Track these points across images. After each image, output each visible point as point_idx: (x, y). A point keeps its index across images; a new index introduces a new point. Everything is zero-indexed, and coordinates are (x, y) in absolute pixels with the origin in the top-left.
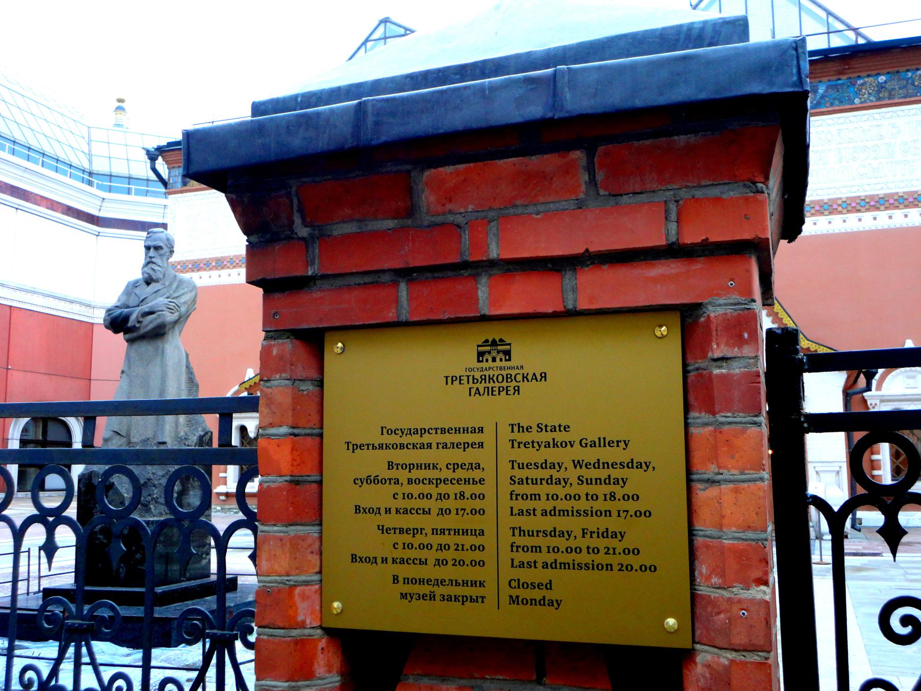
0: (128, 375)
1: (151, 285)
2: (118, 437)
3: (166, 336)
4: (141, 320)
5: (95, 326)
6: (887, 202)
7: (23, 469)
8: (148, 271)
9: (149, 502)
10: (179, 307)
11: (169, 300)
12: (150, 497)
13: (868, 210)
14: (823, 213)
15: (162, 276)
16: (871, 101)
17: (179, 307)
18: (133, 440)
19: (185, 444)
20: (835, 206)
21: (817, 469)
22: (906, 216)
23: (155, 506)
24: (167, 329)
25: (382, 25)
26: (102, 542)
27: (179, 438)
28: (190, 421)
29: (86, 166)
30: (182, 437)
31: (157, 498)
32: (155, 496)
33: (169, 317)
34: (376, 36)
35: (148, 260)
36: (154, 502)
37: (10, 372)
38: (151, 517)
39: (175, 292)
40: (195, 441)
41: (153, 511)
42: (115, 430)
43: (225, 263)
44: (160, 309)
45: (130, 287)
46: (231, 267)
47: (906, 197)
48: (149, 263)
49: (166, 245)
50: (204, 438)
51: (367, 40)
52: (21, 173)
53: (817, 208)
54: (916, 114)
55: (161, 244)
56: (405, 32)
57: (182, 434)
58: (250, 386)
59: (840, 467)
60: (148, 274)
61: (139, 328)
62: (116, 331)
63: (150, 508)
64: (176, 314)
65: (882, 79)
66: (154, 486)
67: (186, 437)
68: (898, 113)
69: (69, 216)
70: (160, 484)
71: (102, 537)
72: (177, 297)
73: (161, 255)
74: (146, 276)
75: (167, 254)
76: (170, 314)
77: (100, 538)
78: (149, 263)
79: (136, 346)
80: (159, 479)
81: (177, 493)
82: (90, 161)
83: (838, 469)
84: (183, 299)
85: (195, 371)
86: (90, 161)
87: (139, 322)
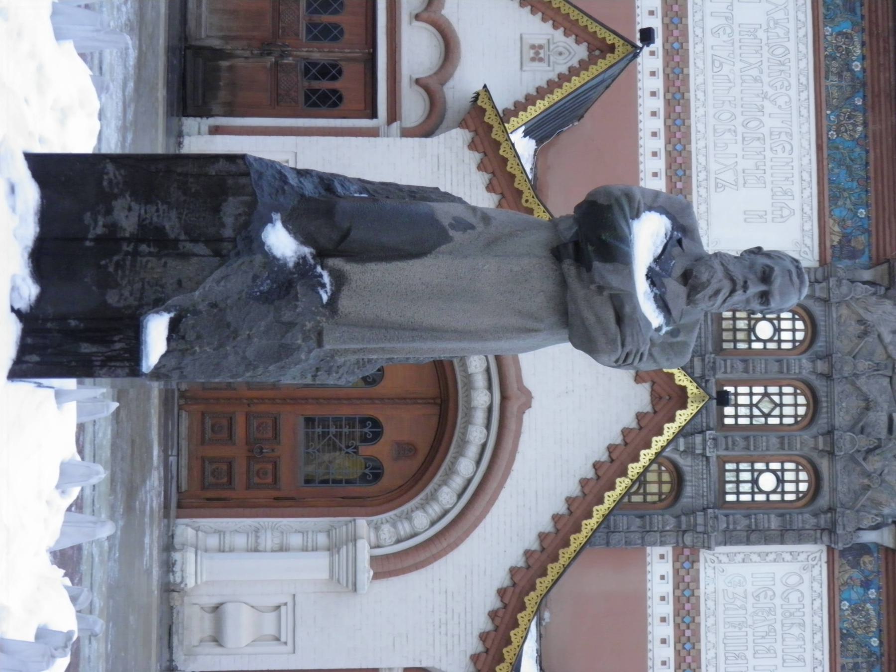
6: (675, 52)
8: (714, 281)
13: (678, 653)
14: (669, 117)
16: (826, 49)
20: (677, 58)
21: (283, 609)
22: (662, 577)
44: (629, 339)
47: (693, 600)
48: (733, 281)
53: (688, 633)
54: (799, 52)
59: (286, 643)
60: (709, 281)
65: (861, 213)
67: (334, 369)
68: (809, 190)
83: (283, 639)
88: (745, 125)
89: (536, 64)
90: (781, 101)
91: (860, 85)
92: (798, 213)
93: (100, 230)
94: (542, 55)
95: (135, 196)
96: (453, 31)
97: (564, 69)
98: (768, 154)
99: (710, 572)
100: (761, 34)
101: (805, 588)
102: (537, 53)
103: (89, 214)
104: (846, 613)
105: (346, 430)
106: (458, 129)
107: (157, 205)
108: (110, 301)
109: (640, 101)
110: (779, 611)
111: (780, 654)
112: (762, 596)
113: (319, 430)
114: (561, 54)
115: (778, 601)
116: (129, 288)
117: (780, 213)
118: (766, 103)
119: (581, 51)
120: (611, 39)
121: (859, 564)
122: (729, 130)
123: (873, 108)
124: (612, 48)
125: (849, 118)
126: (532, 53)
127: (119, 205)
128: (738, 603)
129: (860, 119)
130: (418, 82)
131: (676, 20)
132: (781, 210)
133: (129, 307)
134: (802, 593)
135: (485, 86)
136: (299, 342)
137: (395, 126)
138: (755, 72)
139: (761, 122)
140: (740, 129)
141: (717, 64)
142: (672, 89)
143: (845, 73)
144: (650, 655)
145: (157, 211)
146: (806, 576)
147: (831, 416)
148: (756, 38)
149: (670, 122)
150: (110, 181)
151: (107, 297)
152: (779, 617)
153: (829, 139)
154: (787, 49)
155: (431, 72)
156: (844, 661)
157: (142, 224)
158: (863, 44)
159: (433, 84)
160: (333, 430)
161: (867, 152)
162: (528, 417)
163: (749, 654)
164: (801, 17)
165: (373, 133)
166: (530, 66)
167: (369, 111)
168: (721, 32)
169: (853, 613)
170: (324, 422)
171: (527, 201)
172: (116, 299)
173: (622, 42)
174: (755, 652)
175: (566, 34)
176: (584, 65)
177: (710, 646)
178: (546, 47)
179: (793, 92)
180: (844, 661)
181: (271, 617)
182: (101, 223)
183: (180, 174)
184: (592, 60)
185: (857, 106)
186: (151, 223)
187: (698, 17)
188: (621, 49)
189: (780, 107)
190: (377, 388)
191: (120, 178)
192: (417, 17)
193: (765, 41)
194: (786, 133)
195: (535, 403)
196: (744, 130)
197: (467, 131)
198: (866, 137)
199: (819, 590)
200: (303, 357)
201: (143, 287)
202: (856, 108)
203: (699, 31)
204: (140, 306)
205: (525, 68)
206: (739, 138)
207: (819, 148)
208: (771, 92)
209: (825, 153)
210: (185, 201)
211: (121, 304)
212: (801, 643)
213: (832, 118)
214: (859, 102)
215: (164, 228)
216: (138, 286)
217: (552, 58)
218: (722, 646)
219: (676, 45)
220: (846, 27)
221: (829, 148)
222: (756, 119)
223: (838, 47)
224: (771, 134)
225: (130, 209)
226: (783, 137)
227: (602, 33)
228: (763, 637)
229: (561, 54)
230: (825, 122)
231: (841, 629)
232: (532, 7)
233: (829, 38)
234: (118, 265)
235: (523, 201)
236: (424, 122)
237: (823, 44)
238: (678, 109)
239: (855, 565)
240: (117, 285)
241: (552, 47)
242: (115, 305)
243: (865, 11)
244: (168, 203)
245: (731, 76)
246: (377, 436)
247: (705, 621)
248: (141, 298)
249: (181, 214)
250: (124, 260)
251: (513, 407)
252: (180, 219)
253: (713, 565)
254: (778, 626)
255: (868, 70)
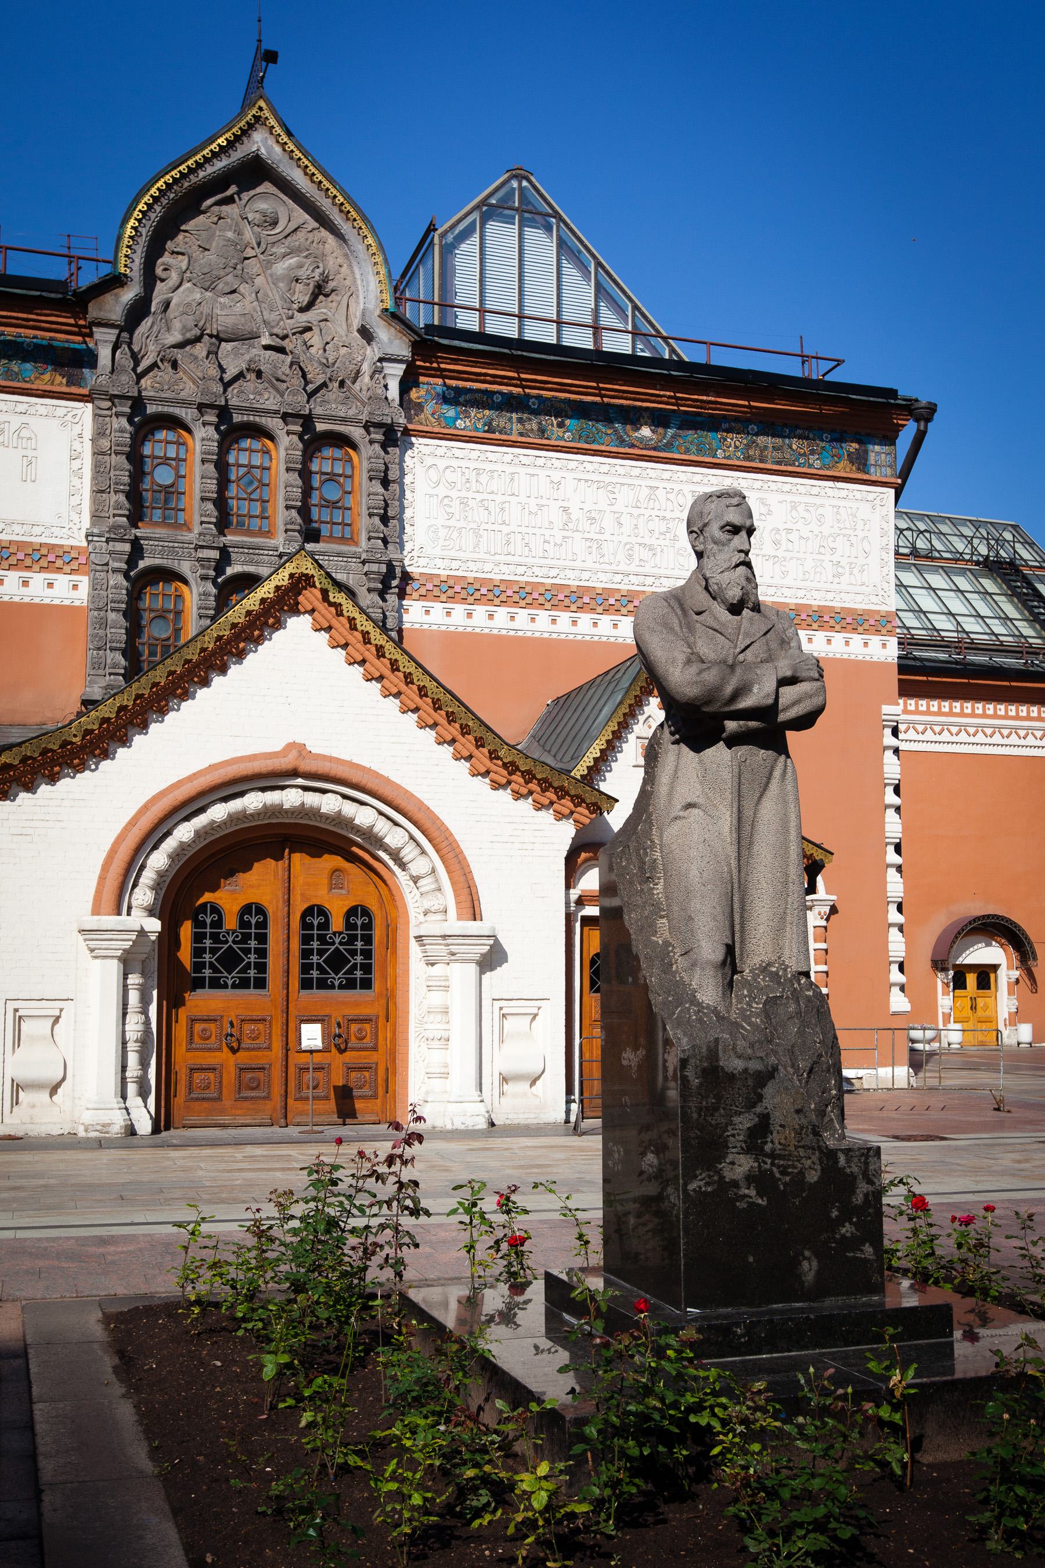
22: (50, 585)
83: (535, 1011)
92: (24, 419)
93: (752, 1192)
95: (721, 1158)
99: (422, 562)
101: (442, 463)
103: (738, 1204)
104: (468, 424)
105: (208, 943)
107: (728, 1136)
108: (815, 1179)
110: (464, 494)
111: (507, 498)
112: (449, 510)
113: (315, 974)
115: (454, 494)
116: (803, 1161)
117: (25, 440)
121: (420, 403)
127: (729, 1175)
128: (455, 535)
132: (22, 438)
133: (820, 1159)
134: (447, 468)
142: (59, 563)
144: (838, 656)
145: (733, 1136)
146: (430, 461)
147: (184, 403)
150: (707, 1184)
151: (812, 1181)
152: (470, 495)
156: (515, 432)
160: (315, 959)
162: (317, 746)
163: (506, 529)
169: (468, 417)
170: (306, 968)
174: (504, 523)
177: (496, 570)
180: (515, 432)
181: (509, 1024)
182: (747, 1191)
183: (700, 1115)
186: (745, 1142)
190: (270, 911)
191: (704, 1175)
195: (299, 740)
199: (511, 457)
201: (803, 1147)
204: (819, 1148)
210: (724, 1109)
212: (496, 474)
215: (749, 1128)
218: (497, 557)
225: (733, 1163)
228: (490, 513)
231: (485, 432)
234: (784, 1173)
239: (420, 407)
240: (801, 1173)
244: (727, 1125)
246: (322, 911)
247: (471, 571)
248: (813, 1149)
249: (735, 1113)
250: (779, 1167)
251: (305, 766)
252: (741, 1113)
253: (416, 559)
254: (479, 497)
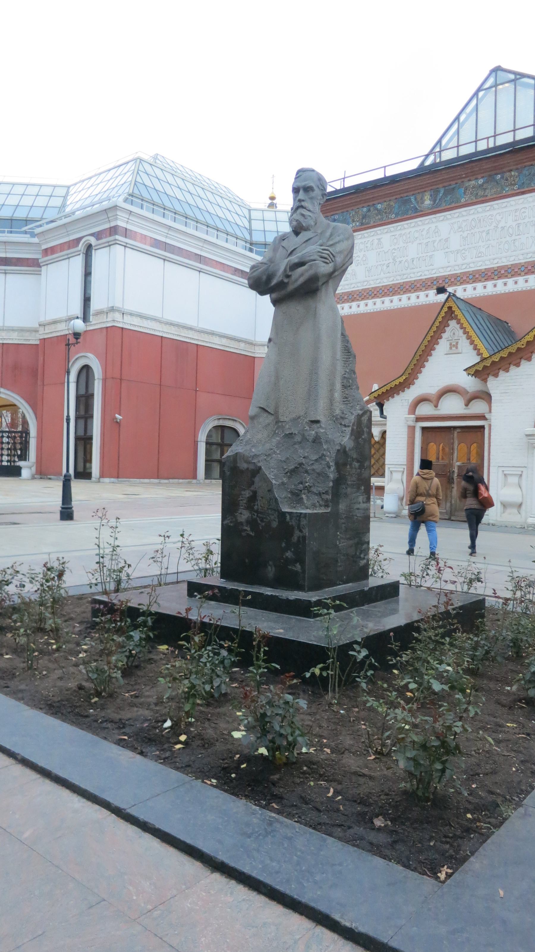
0: (275, 343)
1: (300, 236)
2: (265, 415)
3: (319, 293)
4: (290, 274)
5: (256, 360)
7: (208, 463)
8: (297, 218)
9: (301, 491)
10: (334, 256)
11: (322, 247)
12: (301, 485)
15: (313, 223)
17: (334, 256)
18: (282, 419)
19: (341, 424)
23: (307, 496)
24: (320, 283)
25: (494, 74)
26: (248, 535)
27: (333, 416)
28: (346, 398)
29: (248, 237)
30: (337, 415)
31: (310, 487)
32: (307, 484)
33: (324, 268)
34: (487, 85)
35: (298, 204)
36: (306, 491)
37: (198, 393)
38: (303, 509)
39: (329, 239)
40: (353, 421)
41: (305, 502)
42: (262, 406)
43: (355, 296)
44: (312, 258)
45: (277, 242)
46: (360, 299)
49: (318, 186)
50: (363, 418)
51: (479, 90)
52: (201, 244)
55: (312, 184)
56: (515, 77)
57: (338, 412)
58: (379, 395)
60: (297, 221)
61: (287, 283)
62: (262, 293)
63: (302, 498)
64: (331, 265)
66: (306, 472)
67: (343, 416)
69: (236, 276)
70: (313, 470)
71: (249, 529)
72: (331, 245)
73: (311, 198)
74: (295, 223)
75: (319, 198)
76: (324, 264)
77: (246, 530)
78: (298, 208)
79: (284, 307)
80: (312, 464)
81: (333, 481)
82: (251, 234)
83: (520, 473)
84: (338, 248)
85: (352, 340)
86: (251, 234)
87: (288, 276)
88: (511, 235)
89: (459, 346)
90: (498, 218)
91: (491, 178)
94: (455, 343)
96: (444, 387)
97: (461, 331)
98: (526, 220)
100: (465, 234)
102: (454, 345)
106: (488, 383)
109: (499, 292)
114: (454, 334)
118: (500, 225)
119: (453, 323)
120: (445, 309)
122: (514, 243)
123: (502, 168)
124: (450, 308)
125: (507, 180)
126: (454, 348)
129: (508, 174)
130: (467, 405)
131: (459, 279)
133: (278, 516)
135: (464, 370)
136: (313, 432)
137: (487, 416)
138: (484, 234)
139: (509, 227)
140: (514, 237)
141: (480, 255)
143: (484, 187)
145: (242, 500)
148: (467, 237)
149: (509, 275)
150: (231, 522)
153: (518, 189)
154: (472, 220)
155: (462, 398)
157: (247, 508)
158: (470, 180)
159: (468, 397)
161: (525, 167)
164: (457, 215)
165: (490, 426)
166: (460, 350)
167: (482, 430)
168: (464, 255)
171: (523, 345)
172: (274, 522)
173: (447, 303)
175: (445, 332)
176: (459, 322)
178: (451, 341)
179: (494, 213)
184: (456, 318)
185: (501, 178)
187: (457, 268)
188: (450, 304)
189: (502, 218)
191: (229, 518)
192: (436, 406)
193: (468, 232)
194: (515, 212)
196: (514, 235)
197: (488, 379)
198: (517, 169)
200: (322, 431)
201: (270, 509)
202: (502, 177)
203: (464, 267)
205: (460, 352)
206: (518, 237)
207: (523, 193)
208: (494, 224)
209: (526, 189)
211: (277, 520)
213: (507, 189)
214: (499, 176)
216: (270, 511)
217: (456, 338)
219: (471, 277)
220: (462, 190)
221: (524, 188)
222: (508, 230)
223: (471, 193)
224: (516, 220)
226: (517, 214)
227: (443, 314)
229: (454, 334)
230: (510, 193)
232: (431, 350)
233: (467, 199)
235: (523, 347)
236: (486, 401)
237: (470, 202)
238: (503, 272)
241: (451, 339)
242: (277, 523)
243: (454, 182)
245: (486, 246)
248: (275, 510)
255: (482, 175)
